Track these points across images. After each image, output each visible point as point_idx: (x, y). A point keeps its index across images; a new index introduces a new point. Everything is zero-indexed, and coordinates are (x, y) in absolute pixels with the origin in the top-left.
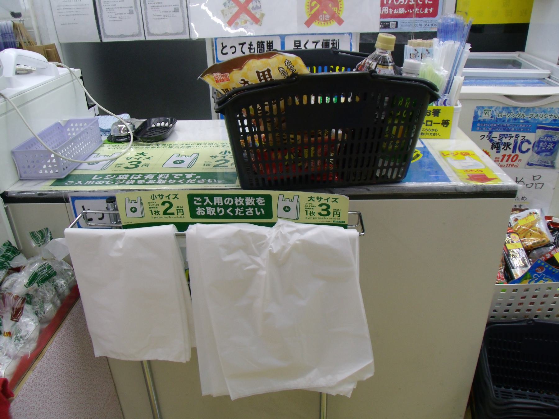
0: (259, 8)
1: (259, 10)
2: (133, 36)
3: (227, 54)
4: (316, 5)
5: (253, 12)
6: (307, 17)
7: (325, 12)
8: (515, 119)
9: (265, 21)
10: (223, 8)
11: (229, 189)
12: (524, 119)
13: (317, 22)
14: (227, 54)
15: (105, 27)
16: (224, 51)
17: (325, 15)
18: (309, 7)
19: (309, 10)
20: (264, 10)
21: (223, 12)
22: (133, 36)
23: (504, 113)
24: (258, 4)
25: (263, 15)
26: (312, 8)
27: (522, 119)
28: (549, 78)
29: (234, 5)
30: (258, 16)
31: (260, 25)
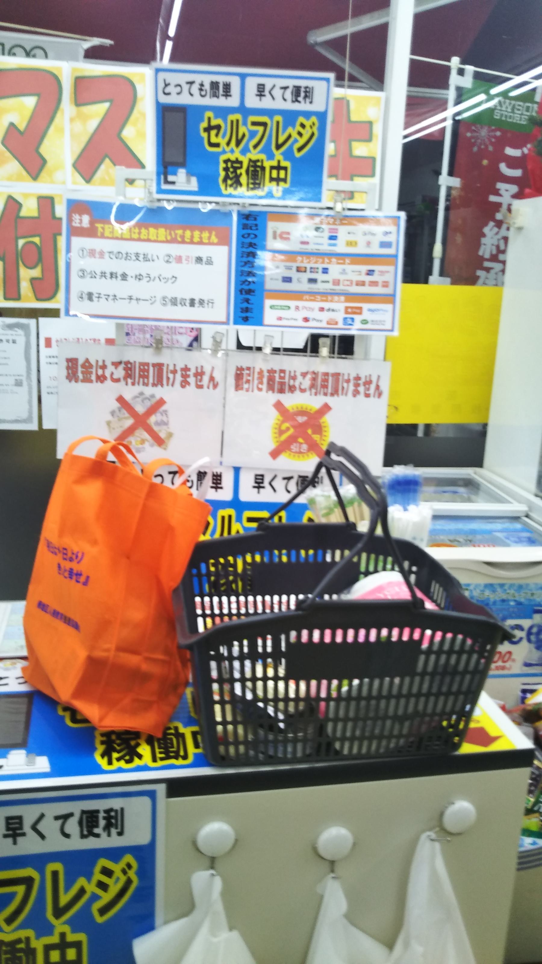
0: (166, 424)
1: (165, 427)
2: (17, 421)
3: (169, 94)
4: (288, 429)
5: (156, 428)
6: (272, 445)
7: (300, 440)
8: (503, 601)
9: (172, 444)
10: (109, 418)
11: (415, 92)
12: (515, 601)
13: (288, 452)
14: (169, 94)
15: (286, 357)
16: (167, 91)
17: (301, 443)
18: (277, 431)
19: (277, 435)
20: (173, 427)
21: (109, 423)
22: (17, 421)
23: (487, 593)
24: (165, 419)
25: (170, 435)
26: (281, 432)
27: (512, 600)
28: (527, 516)
29: (127, 415)
30: (162, 435)
31: (165, 449)
